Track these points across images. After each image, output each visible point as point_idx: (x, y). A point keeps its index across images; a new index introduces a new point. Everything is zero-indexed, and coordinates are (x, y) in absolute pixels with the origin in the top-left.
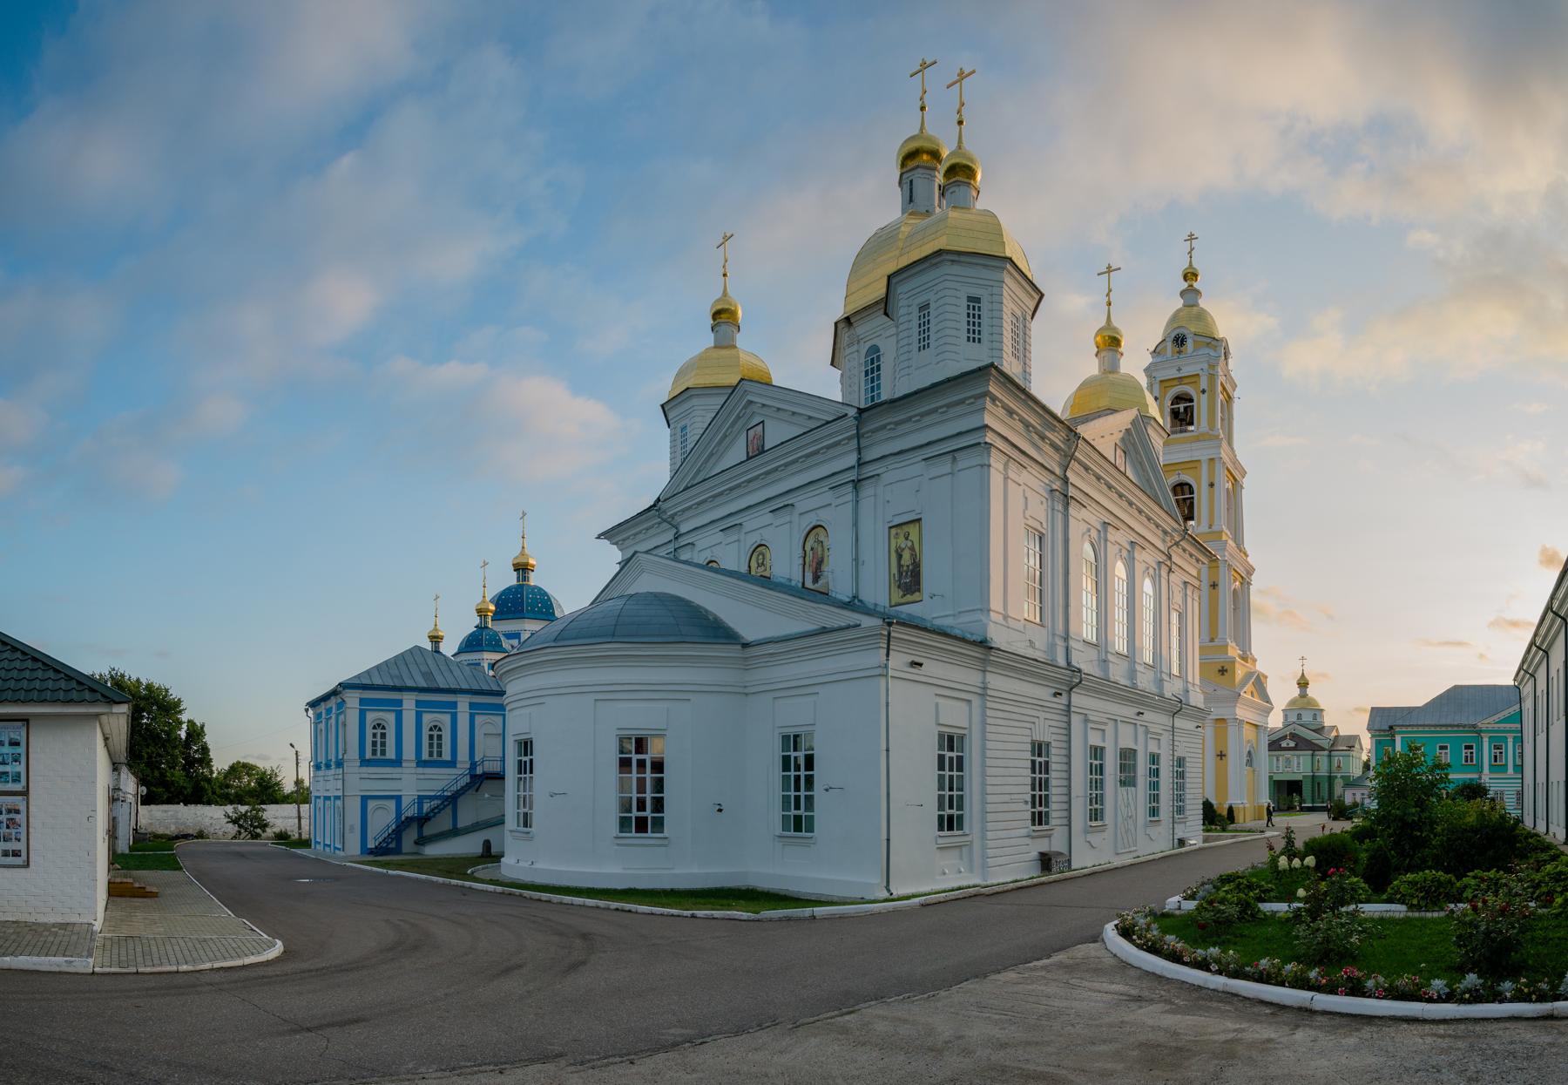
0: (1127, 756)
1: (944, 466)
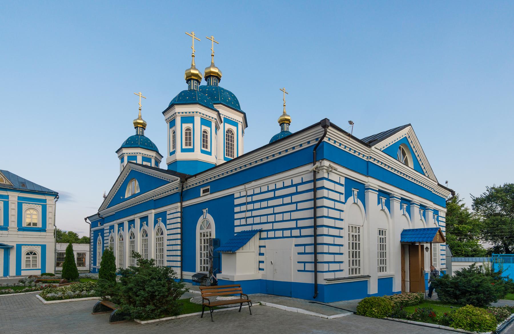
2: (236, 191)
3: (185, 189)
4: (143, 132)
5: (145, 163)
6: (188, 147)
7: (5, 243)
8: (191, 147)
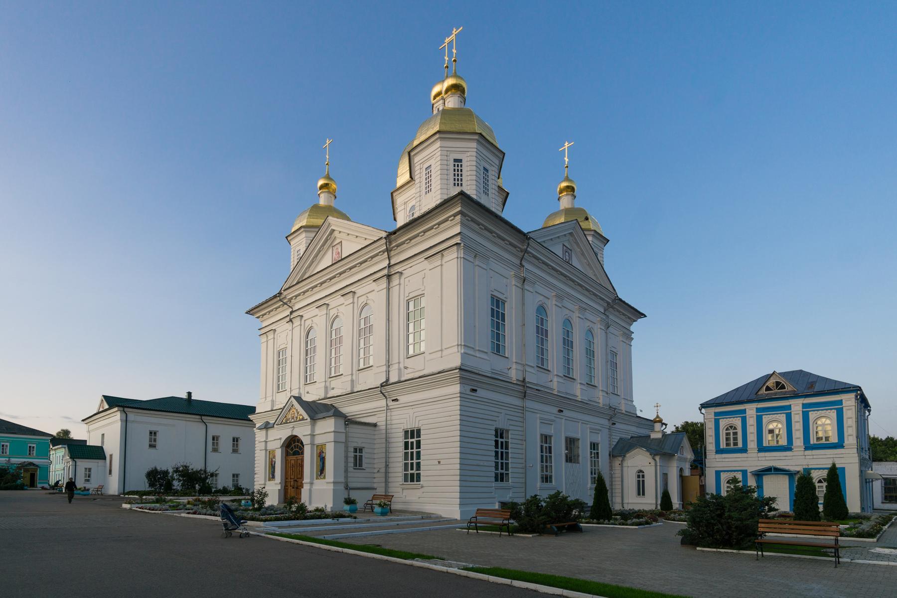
0: (571, 443)
1: (437, 261)
7: (787, 468)
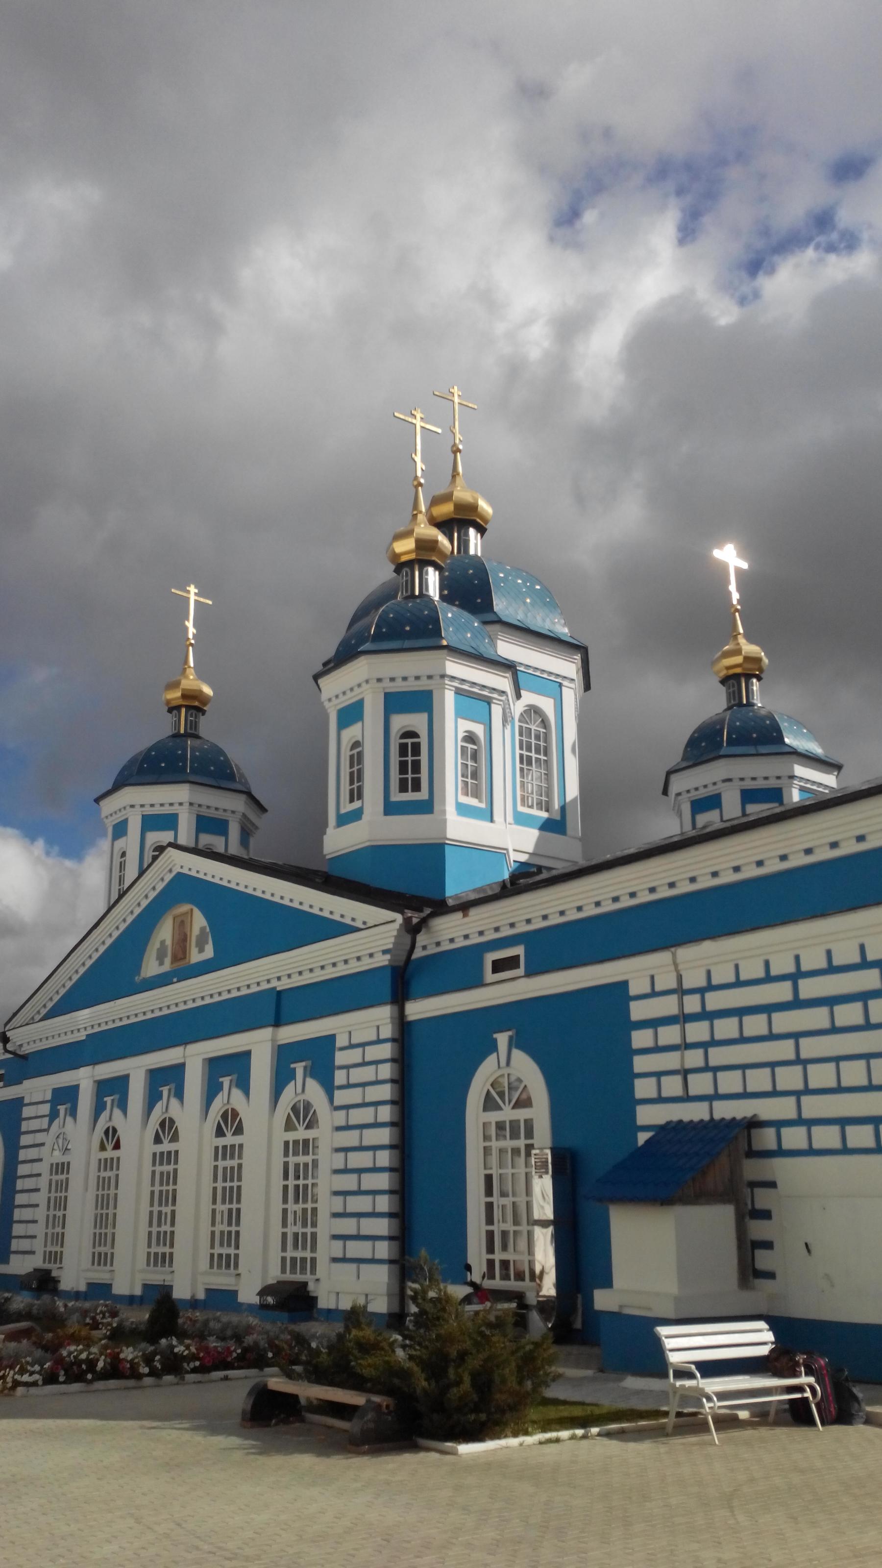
2: (635, 971)
3: (418, 953)
4: (194, 725)
5: (206, 839)
6: (410, 796)
8: (423, 795)
